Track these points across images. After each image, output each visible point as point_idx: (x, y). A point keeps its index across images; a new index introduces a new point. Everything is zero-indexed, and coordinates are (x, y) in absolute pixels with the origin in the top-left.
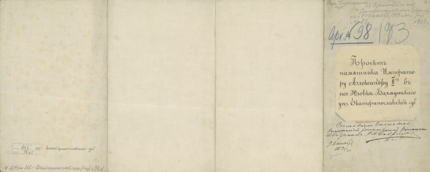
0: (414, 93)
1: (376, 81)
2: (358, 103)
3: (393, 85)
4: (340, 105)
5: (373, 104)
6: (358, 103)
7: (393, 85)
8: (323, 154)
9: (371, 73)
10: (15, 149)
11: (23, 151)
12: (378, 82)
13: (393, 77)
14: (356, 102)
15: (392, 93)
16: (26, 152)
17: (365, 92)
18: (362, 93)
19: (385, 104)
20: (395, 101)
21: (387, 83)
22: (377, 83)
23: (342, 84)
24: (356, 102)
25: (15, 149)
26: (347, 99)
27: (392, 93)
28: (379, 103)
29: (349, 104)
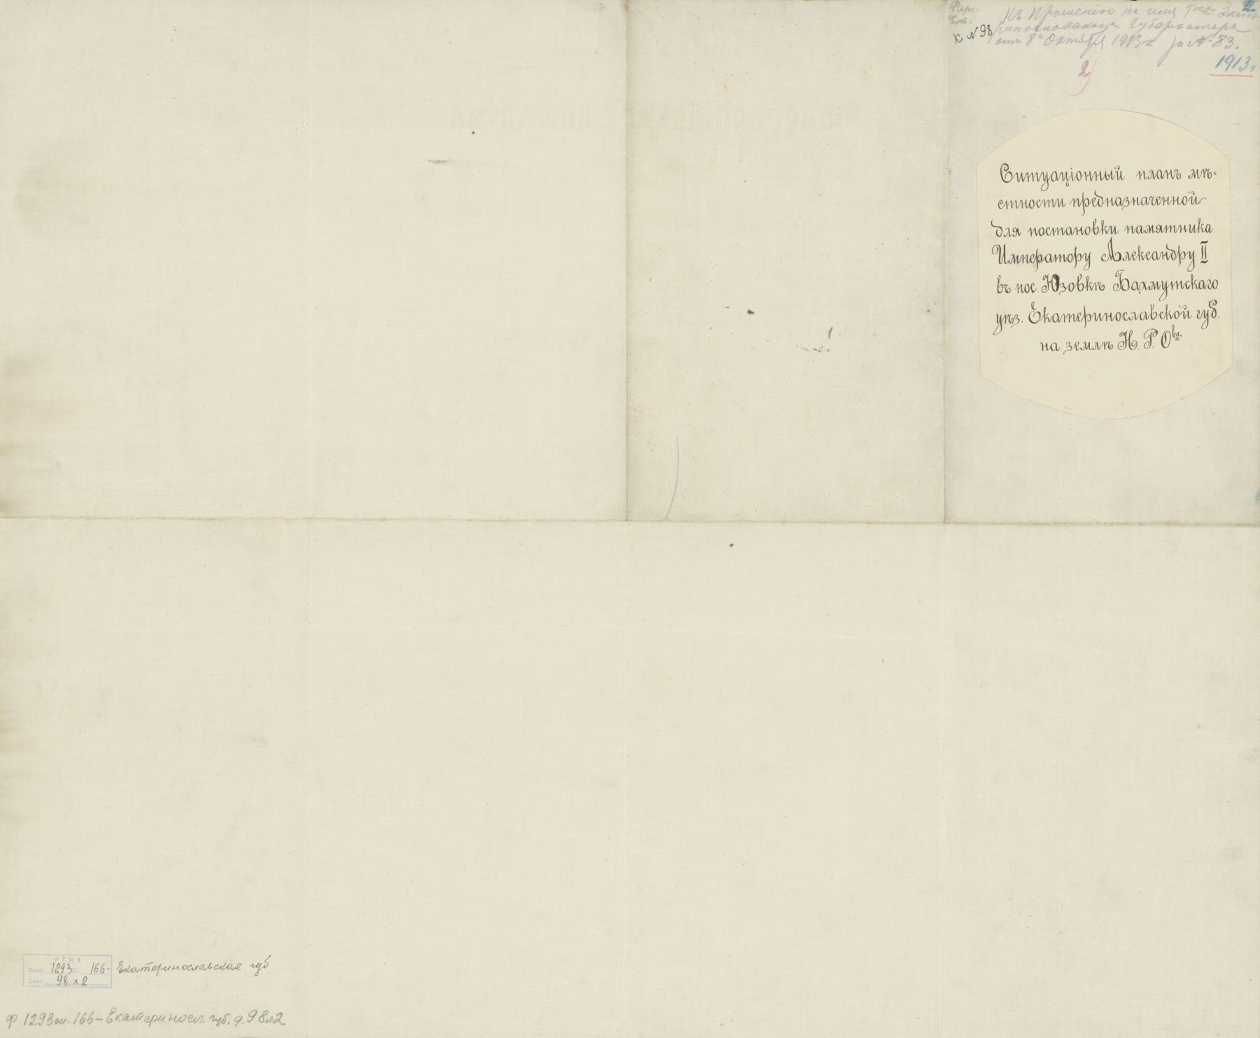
0: (1213, 285)
1: (1165, 251)
2: (1172, 314)
3: (1203, 262)
4: (999, 320)
5: (1093, 318)
6: (1172, 314)
7: (1203, 262)
8: (1177, 524)
9: (1196, 228)
10: (31, 970)
11: (53, 978)
12: (1169, 253)
13: (1203, 242)
14: (1042, 314)
15: (1155, 286)
16: (63, 981)
17: (1083, 281)
18: (1075, 283)
19: (1126, 317)
20: (1158, 309)
21: (1193, 254)
22: (1169, 255)
23: (1183, 255)
24: (1042, 314)
25: (31, 970)
26: (1018, 304)
27: (1155, 286)
28: (1109, 315)
29: (1024, 318)
